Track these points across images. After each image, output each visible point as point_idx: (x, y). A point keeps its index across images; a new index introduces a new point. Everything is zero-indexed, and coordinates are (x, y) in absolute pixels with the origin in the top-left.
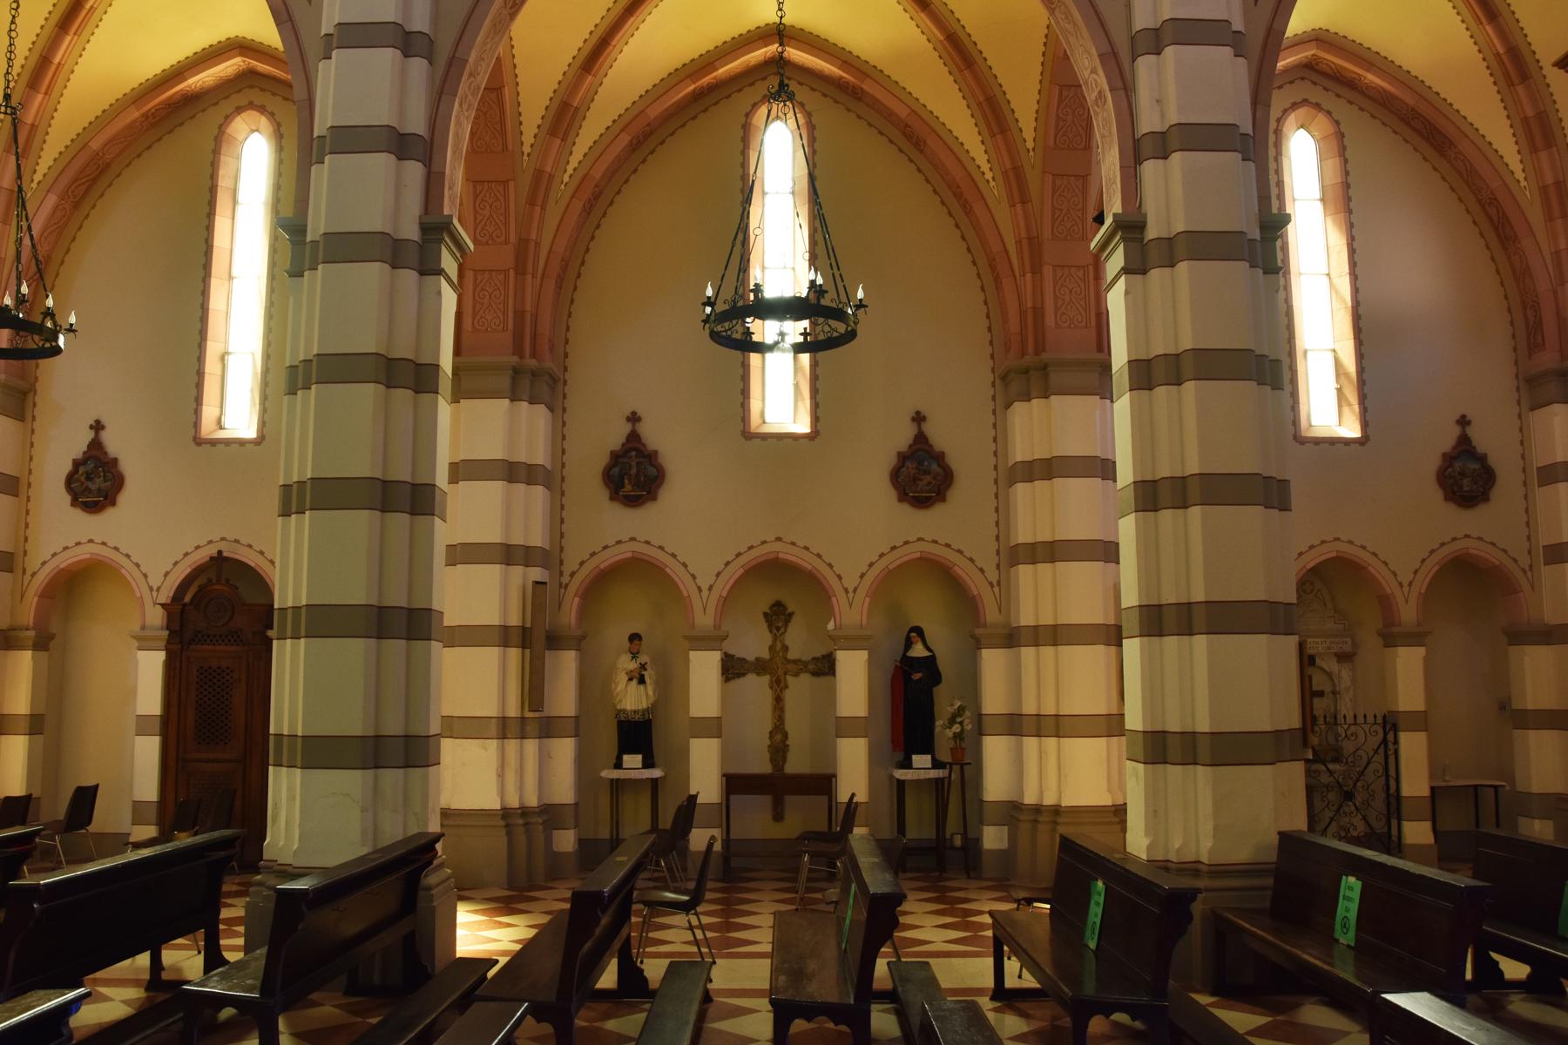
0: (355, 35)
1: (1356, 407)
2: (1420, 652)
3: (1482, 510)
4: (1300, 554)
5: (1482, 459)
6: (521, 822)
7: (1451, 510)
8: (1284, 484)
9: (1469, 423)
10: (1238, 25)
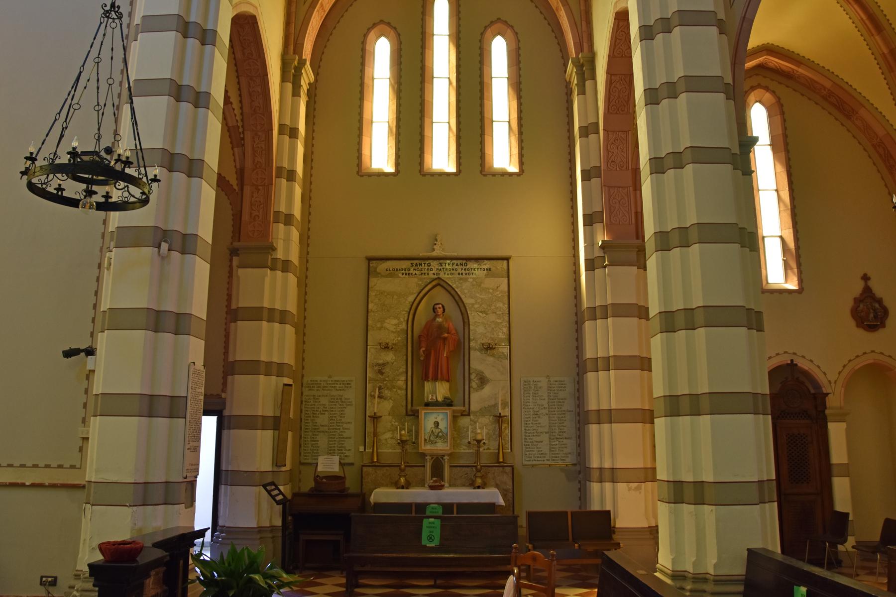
0: (152, 24)
1: (796, 270)
2: (843, 425)
3: (881, 333)
4: (770, 358)
5: (880, 301)
6: (270, 535)
7: (861, 333)
8: (759, 313)
9: (869, 279)
10: (721, 15)
